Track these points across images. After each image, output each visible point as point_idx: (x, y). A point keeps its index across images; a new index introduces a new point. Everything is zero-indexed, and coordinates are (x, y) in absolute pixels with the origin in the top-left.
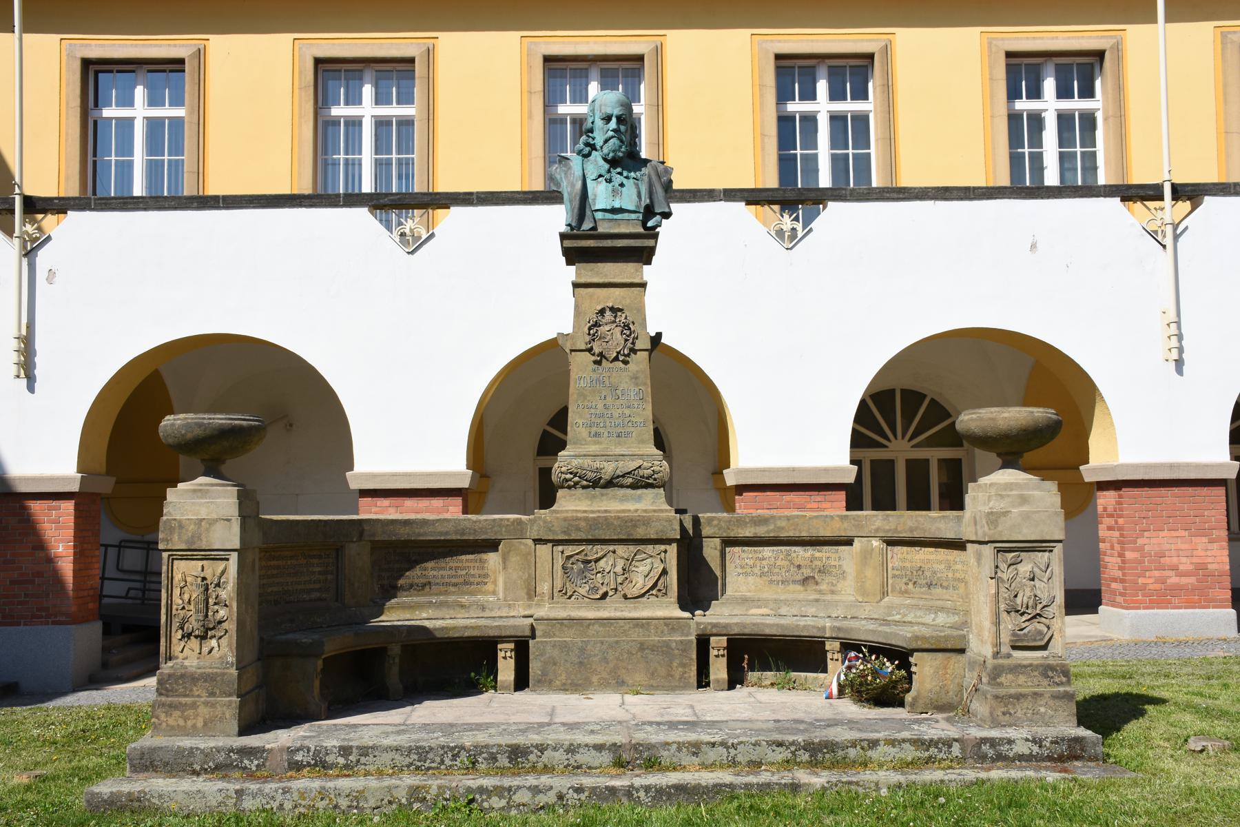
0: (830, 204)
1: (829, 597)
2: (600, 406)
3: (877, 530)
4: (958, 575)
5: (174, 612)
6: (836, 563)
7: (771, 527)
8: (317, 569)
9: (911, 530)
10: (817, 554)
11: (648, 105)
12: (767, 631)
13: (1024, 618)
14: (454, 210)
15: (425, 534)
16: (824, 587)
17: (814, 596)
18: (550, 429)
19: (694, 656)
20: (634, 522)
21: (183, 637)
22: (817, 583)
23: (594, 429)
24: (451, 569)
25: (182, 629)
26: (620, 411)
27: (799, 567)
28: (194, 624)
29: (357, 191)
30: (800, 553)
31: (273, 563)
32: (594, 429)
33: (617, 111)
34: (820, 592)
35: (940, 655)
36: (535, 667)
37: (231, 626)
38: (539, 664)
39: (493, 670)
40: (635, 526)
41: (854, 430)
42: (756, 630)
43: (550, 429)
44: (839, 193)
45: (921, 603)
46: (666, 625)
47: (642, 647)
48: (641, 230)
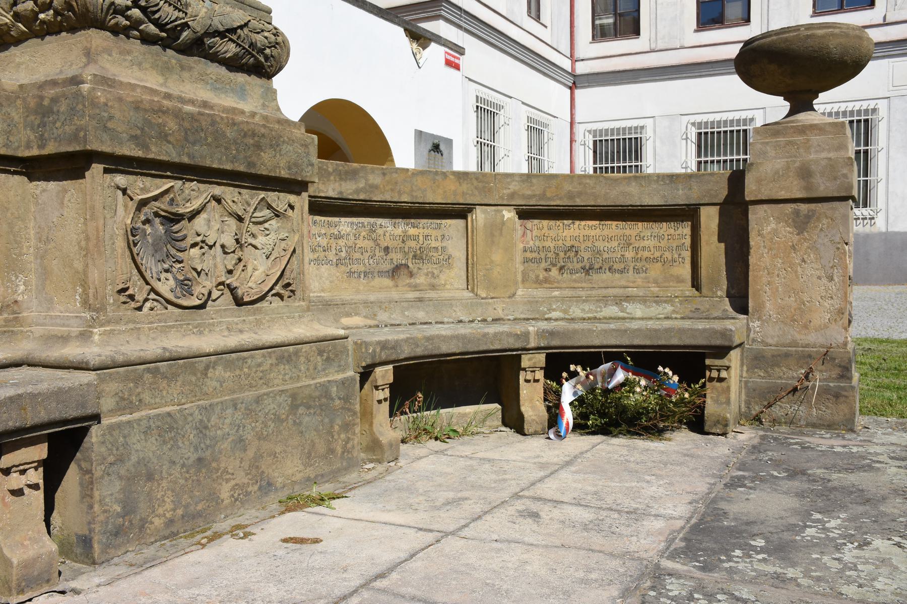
1: (432, 294)
3: (512, 195)
4: (646, 254)
7: (362, 185)
9: (571, 196)
10: (412, 231)
12: (445, 349)
16: (421, 280)
17: (411, 295)
22: (411, 275)
27: (387, 249)
30: (390, 229)
34: (415, 288)
38: (118, 485)
40: (258, 147)
42: (431, 349)
45: (582, 293)
46: (320, 353)
47: (296, 401)
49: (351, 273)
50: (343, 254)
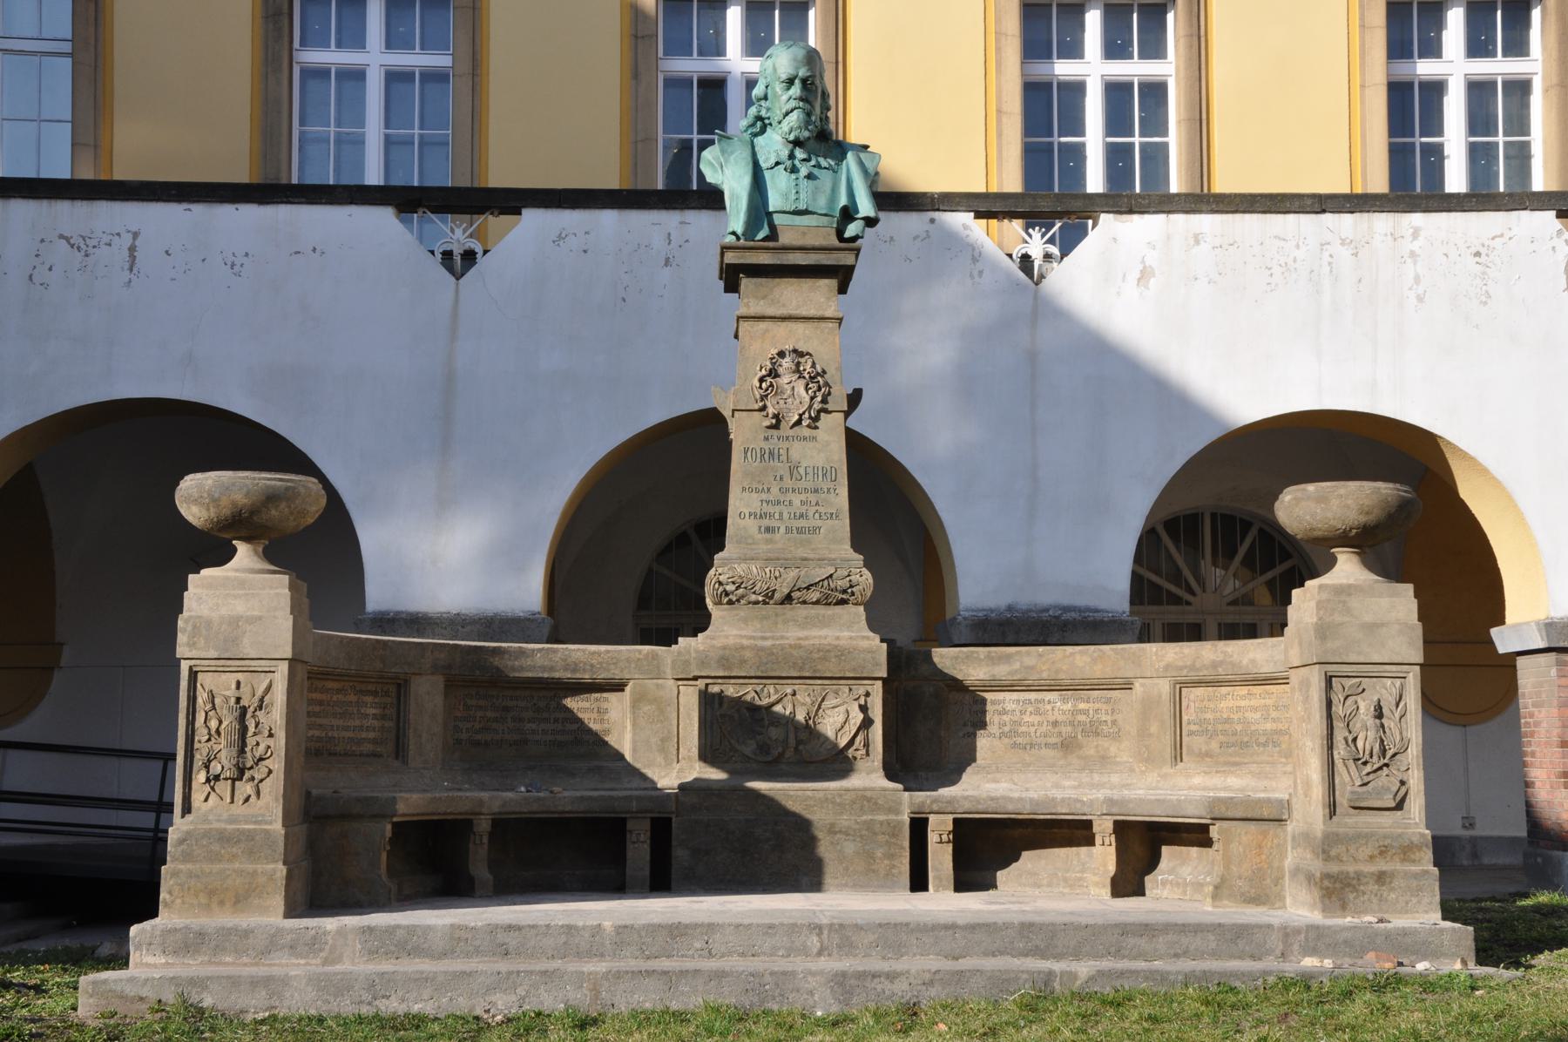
2: (775, 490)
3: (1167, 667)
5: (196, 745)
6: (1109, 718)
7: (1017, 666)
8: (372, 711)
10: (1082, 706)
13: (1368, 768)
14: (528, 213)
15: (522, 668)
19: (907, 844)
20: (825, 652)
21: (208, 780)
23: (766, 522)
24: (556, 720)
25: (207, 767)
26: (803, 497)
28: (224, 763)
29: (295, 181)
32: (766, 522)
33: (803, 72)
35: (1252, 826)
36: (680, 854)
37: (277, 764)
39: (620, 857)
41: (1134, 573)
42: (992, 806)
44: (1120, 200)
48: (835, 242)
49: (1015, 745)
50: (1006, 729)
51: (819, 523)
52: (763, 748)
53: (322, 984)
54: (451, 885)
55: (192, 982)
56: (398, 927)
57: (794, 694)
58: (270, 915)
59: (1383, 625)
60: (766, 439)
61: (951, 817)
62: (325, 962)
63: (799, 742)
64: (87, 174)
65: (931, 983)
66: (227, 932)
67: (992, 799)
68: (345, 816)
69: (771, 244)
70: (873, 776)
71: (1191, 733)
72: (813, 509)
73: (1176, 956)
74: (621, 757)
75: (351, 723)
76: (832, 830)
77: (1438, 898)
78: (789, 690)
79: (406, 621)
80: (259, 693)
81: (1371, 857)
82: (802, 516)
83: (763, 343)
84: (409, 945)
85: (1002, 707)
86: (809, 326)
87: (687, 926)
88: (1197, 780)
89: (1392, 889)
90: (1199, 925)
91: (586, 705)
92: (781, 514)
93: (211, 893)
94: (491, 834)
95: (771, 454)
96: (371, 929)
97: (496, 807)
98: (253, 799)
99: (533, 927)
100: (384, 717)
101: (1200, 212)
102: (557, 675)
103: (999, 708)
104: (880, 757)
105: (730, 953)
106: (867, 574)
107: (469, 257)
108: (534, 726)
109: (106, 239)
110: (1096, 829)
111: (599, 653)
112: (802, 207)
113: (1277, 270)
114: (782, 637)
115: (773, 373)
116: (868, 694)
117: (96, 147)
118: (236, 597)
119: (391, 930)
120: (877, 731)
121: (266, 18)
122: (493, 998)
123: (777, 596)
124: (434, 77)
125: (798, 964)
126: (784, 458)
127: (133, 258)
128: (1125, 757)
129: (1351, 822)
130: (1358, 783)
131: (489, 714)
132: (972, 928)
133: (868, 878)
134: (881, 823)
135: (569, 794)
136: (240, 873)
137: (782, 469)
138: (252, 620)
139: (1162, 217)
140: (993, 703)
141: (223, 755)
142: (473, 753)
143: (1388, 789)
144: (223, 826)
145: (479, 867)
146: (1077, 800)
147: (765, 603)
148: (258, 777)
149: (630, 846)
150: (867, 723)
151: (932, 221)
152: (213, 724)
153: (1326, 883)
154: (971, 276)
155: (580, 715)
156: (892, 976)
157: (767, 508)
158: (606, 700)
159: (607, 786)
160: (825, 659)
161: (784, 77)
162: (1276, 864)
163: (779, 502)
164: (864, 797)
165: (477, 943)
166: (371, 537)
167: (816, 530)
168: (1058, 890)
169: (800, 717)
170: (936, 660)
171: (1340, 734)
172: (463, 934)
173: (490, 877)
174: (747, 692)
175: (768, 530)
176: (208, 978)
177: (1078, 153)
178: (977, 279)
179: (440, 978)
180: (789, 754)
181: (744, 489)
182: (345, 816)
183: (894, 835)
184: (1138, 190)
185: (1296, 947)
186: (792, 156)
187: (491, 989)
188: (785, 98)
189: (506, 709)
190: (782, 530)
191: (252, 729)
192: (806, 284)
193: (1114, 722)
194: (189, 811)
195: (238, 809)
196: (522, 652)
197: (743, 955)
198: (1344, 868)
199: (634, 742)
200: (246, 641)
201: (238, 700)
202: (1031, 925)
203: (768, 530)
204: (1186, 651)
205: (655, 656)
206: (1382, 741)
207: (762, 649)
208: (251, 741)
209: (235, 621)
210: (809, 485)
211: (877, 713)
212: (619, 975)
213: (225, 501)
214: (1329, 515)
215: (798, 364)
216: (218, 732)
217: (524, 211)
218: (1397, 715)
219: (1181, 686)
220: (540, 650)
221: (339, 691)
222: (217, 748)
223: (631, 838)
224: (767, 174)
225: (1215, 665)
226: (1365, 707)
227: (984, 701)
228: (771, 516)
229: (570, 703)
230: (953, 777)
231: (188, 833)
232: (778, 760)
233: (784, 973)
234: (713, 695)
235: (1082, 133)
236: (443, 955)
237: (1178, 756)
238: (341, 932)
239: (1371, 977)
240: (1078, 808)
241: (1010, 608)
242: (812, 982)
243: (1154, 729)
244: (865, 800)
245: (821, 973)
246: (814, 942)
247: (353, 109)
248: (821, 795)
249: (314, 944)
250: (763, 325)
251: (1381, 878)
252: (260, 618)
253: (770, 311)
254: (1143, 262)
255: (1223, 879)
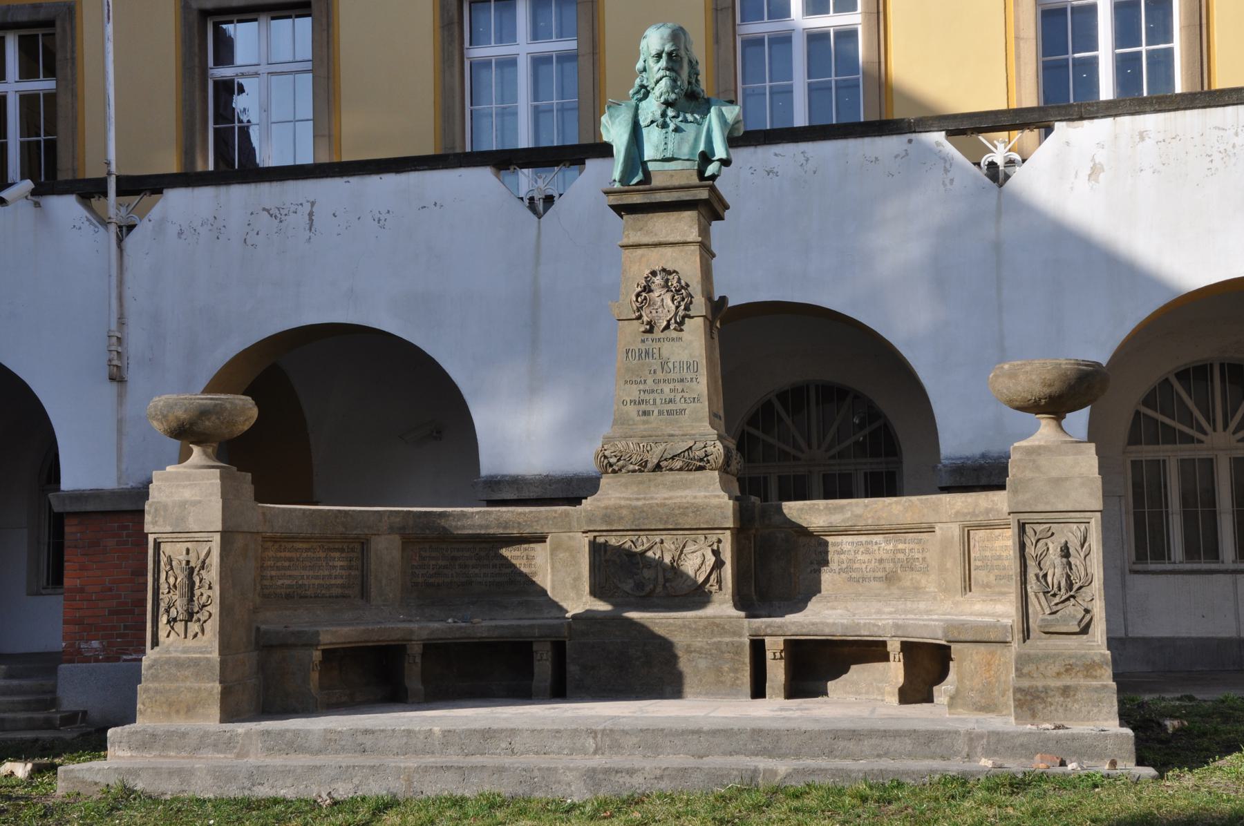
0: (1059, 126)
2: (650, 381)
3: (957, 513)
5: (161, 596)
7: (849, 514)
10: (900, 546)
11: (866, 13)
13: (1057, 600)
15: (464, 527)
18: (747, 428)
19: (747, 660)
20: (685, 509)
21: (169, 622)
23: (643, 407)
24: (494, 566)
25: (167, 611)
26: (672, 386)
28: (179, 609)
29: (468, 149)
31: (283, 554)
32: (643, 407)
33: (668, 48)
35: (982, 647)
36: (572, 669)
37: (214, 609)
42: (813, 630)
43: (747, 428)
48: (695, 180)
50: (844, 566)
51: (684, 406)
52: (640, 586)
53: (218, 774)
54: (393, 695)
55: (130, 772)
56: (287, 730)
57: (662, 542)
58: (210, 721)
59: (1067, 479)
60: (643, 341)
61: (782, 639)
62: (238, 756)
63: (666, 580)
64: (324, 159)
65: (662, 777)
66: (170, 734)
67: (813, 624)
68: (284, 646)
69: (647, 187)
70: (724, 606)
71: (977, 568)
72: (680, 395)
73: (879, 756)
74: (544, 592)
75: (321, 573)
76: (689, 650)
77: (1116, 708)
78: (658, 540)
79: (508, 482)
80: (202, 556)
81: (1058, 674)
82: (670, 401)
83: (640, 266)
84: (294, 745)
85: (840, 547)
86: (677, 249)
87: (495, 731)
88: (978, 607)
89: (1076, 701)
90: (897, 731)
91: (517, 553)
92: (655, 400)
93: (170, 705)
94: (423, 655)
95: (647, 353)
96: (268, 733)
97: (424, 635)
98: (200, 635)
99: (383, 731)
100: (350, 568)
101: (1144, 112)
102: (491, 531)
103: (838, 548)
104: (730, 591)
105: (527, 752)
106: (719, 445)
107: (549, 200)
108: (477, 571)
109: (293, 208)
110: (889, 648)
111: (525, 514)
112: (668, 155)
113: (1217, 157)
114: (652, 498)
115: (647, 289)
116: (719, 541)
117: (330, 136)
118: (184, 487)
119: (282, 733)
120: (728, 571)
121: (443, 27)
122: (336, 786)
123: (650, 465)
124: (564, 58)
125: (561, 762)
126: (657, 355)
127: (311, 220)
128: (932, 588)
129: (1039, 644)
130: (1048, 611)
131: (441, 563)
132: (714, 733)
133: (719, 688)
134: (727, 644)
135: (487, 624)
136: (190, 689)
137: (655, 364)
138: (194, 503)
139: (1111, 119)
140: (834, 544)
141: (178, 603)
142: (426, 593)
143: (1074, 617)
144: (179, 655)
145: (413, 681)
146: (875, 625)
147: (640, 471)
148: (203, 619)
149: (536, 663)
150: (719, 564)
151: (910, 141)
152: (172, 580)
153: (1019, 696)
154: (944, 184)
155: (514, 562)
156: (631, 772)
157: (643, 396)
158: (533, 549)
159: (531, 616)
160: (684, 514)
161: (654, 52)
162: (1003, 678)
163: (653, 391)
164: (714, 624)
165: (343, 743)
166: (482, 418)
167: (682, 411)
168: (864, 698)
169: (667, 560)
170: (785, 511)
171: (1032, 571)
172: (333, 737)
173: (420, 687)
174: (625, 541)
175: (645, 413)
176: (140, 769)
177: (1092, 64)
178: (949, 186)
179: (299, 771)
180: (659, 589)
181: (626, 382)
182: (284, 646)
183: (737, 653)
184: (1145, 94)
185: (979, 749)
186: (664, 115)
187: (334, 780)
188: (656, 69)
189: (454, 558)
190: (656, 412)
191: (197, 584)
192: (673, 216)
193: (924, 559)
194: (157, 645)
195: (190, 642)
196: (463, 514)
197: (537, 753)
198: (1034, 683)
199: (553, 581)
200: (191, 519)
201: (188, 562)
202: (761, 731)
203: (645, 413)
204: (969, 500)
205: (567, 514)
206: (1068, 577)
207: (636, 508)
208: (197, 592)
209: (183, 505)
210: (676, 376)
211: (727, 556)
212: (426, 769)
213: (171, 417)
214: (1020, 388)
215: (667, 280)
216: (175, 586)
217: (588, 162)
218: (1082, 555)
219: (967, 532)
220: (478, 513)
221: (307, 550)
222: (175, 598)
223: (537, 657)
224: (645, 131)
225: (988, 511)
226: (1054, 547)
227: (826, 543)
228: (647, 402)
229: (505, 552)
230: (799, 604)
231: (155, 660)
232: (650, 595)
233: (549, 769)
234: (600, 544)
235: (1095, 48)
236: (319, 752)
237: (967, 586)
238: (247, 734)
239: (1020, 776)
240: (875, 631)
241: (983, 456)
242: (570, 776)
243: (949, 565)
244: (716, 626)
245: (577, 769)
246: (590, 743)
247: (507, 92)
248: (680, 622)
249: (228, 744)
250: (640, 251)
251: (1066, 691)
252: (200, 502)
253: (645, 240)
254: (1093, 160)
255: (957, 690)
